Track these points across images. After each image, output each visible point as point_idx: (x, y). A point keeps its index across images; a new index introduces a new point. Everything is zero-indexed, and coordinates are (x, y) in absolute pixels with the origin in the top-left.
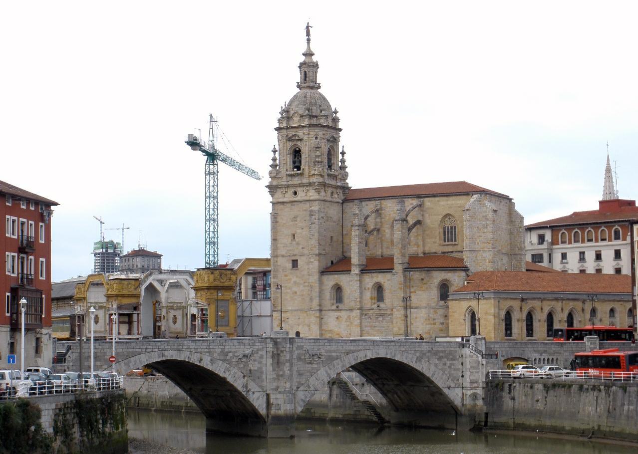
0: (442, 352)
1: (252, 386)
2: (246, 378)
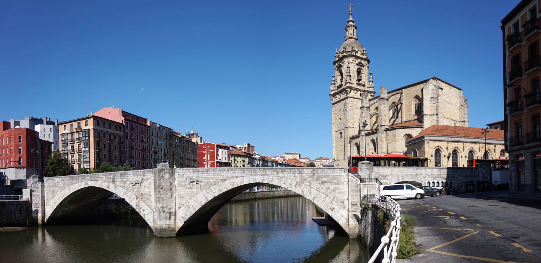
0: (325, 177)
1: (142, 204)
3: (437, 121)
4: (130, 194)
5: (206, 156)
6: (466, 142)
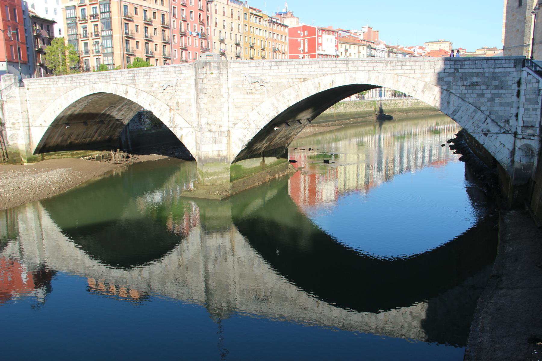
0: (477, 75)
5: (302, 45)
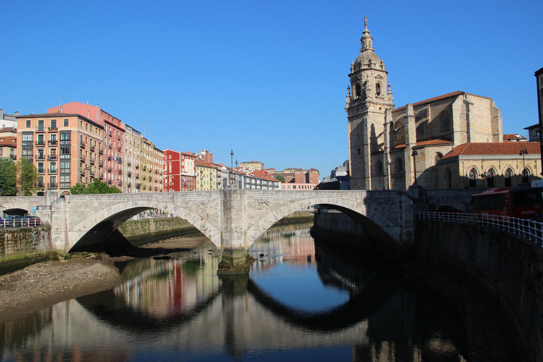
1: (208, 225)
2: (204, 220)
3: (469, 138)
4: (193, 215)
6: (502, 160)
